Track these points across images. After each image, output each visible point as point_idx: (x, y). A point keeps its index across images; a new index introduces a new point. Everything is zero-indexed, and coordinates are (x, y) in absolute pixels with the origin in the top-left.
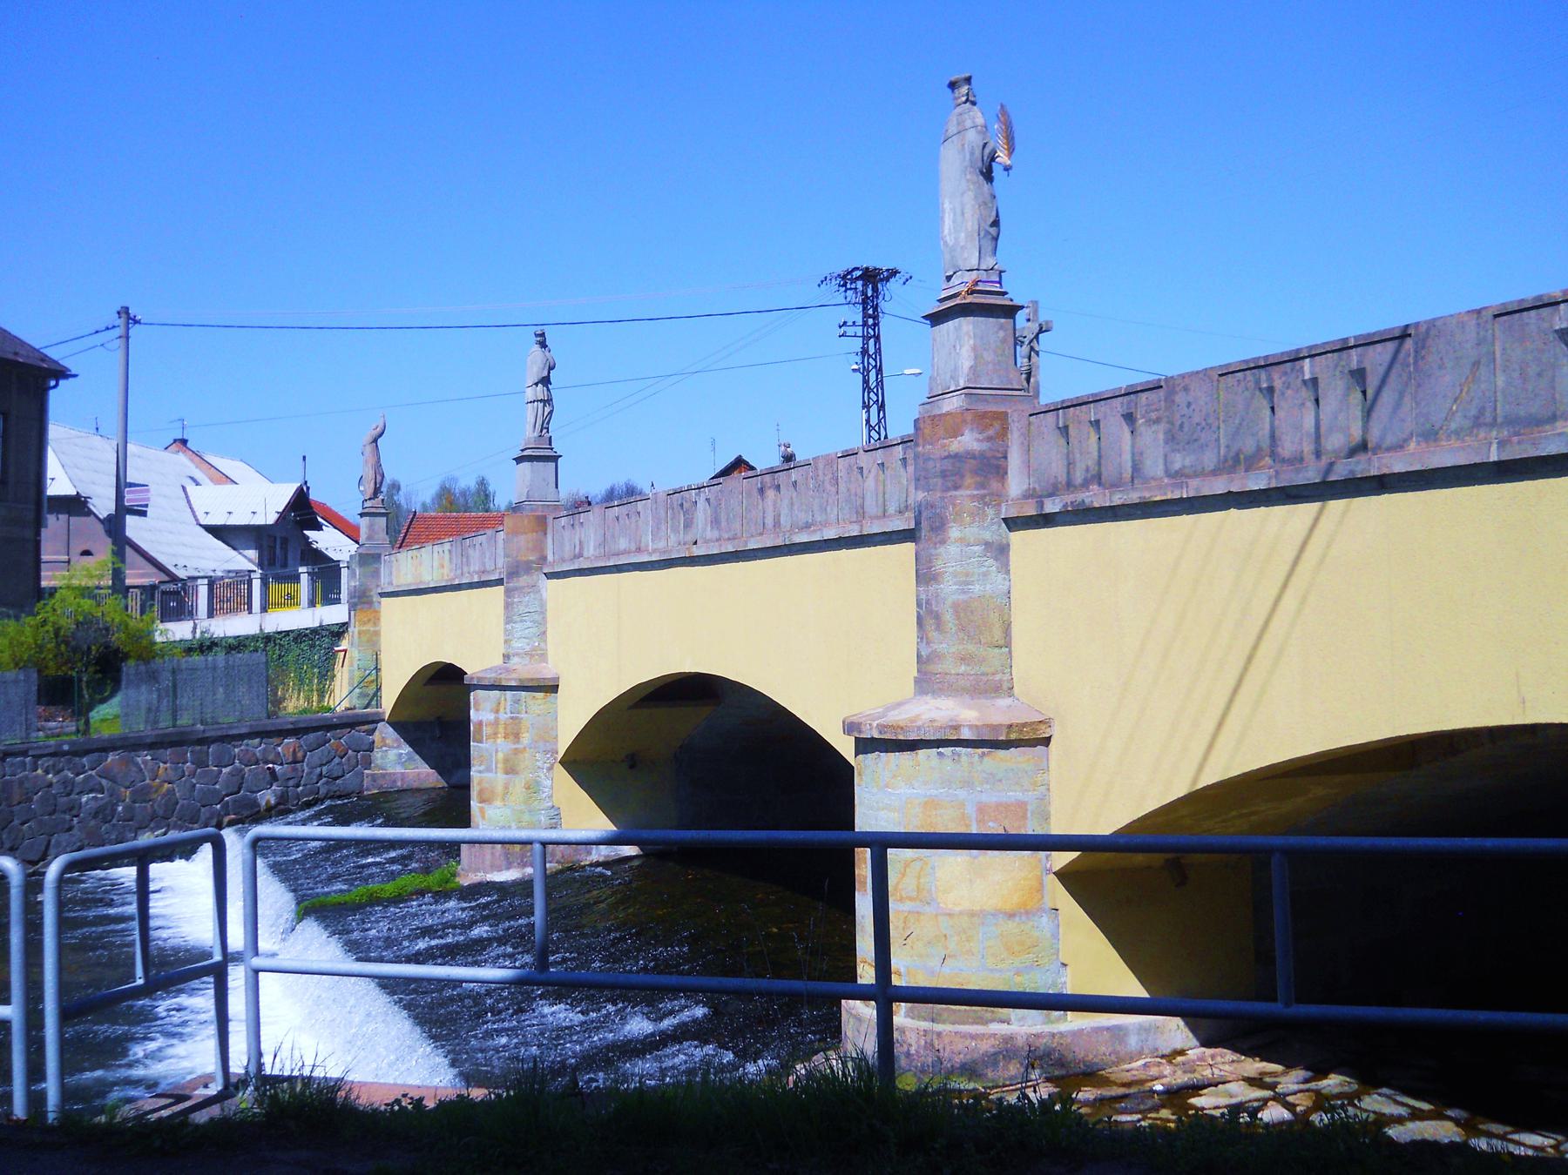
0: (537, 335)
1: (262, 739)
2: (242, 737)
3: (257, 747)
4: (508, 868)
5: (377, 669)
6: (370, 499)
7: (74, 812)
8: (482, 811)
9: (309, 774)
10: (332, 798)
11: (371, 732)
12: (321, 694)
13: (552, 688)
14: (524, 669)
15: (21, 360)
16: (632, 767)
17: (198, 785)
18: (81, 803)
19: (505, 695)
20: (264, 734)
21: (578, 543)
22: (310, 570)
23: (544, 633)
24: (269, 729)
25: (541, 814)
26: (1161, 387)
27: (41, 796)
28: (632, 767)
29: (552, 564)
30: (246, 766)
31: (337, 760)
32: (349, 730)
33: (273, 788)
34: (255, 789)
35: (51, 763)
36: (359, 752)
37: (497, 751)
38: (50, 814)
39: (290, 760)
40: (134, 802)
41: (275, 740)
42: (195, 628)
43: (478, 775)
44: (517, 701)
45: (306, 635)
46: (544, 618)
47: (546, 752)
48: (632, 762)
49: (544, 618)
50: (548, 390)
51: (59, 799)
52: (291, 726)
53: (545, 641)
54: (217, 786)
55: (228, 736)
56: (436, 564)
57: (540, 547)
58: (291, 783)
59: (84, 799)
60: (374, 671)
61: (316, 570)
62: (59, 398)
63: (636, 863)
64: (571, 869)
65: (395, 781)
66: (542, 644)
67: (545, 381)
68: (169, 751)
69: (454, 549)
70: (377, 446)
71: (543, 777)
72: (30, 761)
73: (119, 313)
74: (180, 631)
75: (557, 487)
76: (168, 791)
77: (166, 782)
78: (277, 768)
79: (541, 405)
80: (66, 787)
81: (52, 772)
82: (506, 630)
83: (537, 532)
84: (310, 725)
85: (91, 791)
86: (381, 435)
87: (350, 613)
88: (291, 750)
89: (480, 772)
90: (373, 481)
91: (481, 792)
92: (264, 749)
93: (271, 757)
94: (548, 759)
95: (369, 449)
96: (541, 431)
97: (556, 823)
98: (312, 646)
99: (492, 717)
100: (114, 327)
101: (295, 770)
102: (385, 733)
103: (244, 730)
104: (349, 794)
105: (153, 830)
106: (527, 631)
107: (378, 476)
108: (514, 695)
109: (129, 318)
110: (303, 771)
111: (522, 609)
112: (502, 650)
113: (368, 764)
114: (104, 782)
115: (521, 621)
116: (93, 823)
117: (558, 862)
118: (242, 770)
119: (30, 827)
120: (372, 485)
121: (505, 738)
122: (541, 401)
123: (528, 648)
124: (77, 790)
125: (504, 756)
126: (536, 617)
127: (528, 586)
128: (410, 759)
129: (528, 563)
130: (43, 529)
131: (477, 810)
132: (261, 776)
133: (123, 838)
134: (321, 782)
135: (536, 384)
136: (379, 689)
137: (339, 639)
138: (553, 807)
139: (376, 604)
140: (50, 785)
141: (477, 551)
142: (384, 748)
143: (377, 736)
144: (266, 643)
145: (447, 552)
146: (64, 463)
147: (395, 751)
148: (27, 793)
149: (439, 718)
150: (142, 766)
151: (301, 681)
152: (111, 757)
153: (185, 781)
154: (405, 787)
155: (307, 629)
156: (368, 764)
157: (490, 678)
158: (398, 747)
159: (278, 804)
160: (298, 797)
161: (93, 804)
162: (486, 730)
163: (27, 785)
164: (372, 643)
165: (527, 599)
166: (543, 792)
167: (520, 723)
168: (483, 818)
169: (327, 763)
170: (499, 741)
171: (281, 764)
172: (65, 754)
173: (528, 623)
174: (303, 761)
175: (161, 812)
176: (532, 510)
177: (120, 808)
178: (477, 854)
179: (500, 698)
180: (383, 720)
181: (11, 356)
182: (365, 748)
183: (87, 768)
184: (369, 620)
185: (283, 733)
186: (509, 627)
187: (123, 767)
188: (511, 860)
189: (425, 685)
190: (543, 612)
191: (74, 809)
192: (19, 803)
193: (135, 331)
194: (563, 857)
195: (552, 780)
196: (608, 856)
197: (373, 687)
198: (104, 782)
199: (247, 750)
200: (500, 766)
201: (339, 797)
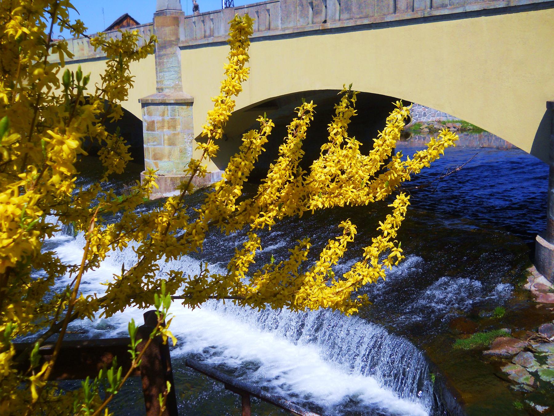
13: (190, 104)
23: (180, 77)
26: (395, 12)
29: (183, 42)
37: (164, 135)
44: (174, 110)
49: (180, 70)
53: (181, 81)
57: (176, 34)
66: (180, 83)
83: (174, 25)
94: (190, 137)
99: (160, 118)
106: (172, 76)
115: (169, 71)
121: (168, 128)
123: (173, 85)
126: (176, 69)
129: (170, 41)
157: (160, 99)
167: (176, 121)
170: (165, 130)
176: (171, 14)
179: (165, 109)
190: (179, 67)
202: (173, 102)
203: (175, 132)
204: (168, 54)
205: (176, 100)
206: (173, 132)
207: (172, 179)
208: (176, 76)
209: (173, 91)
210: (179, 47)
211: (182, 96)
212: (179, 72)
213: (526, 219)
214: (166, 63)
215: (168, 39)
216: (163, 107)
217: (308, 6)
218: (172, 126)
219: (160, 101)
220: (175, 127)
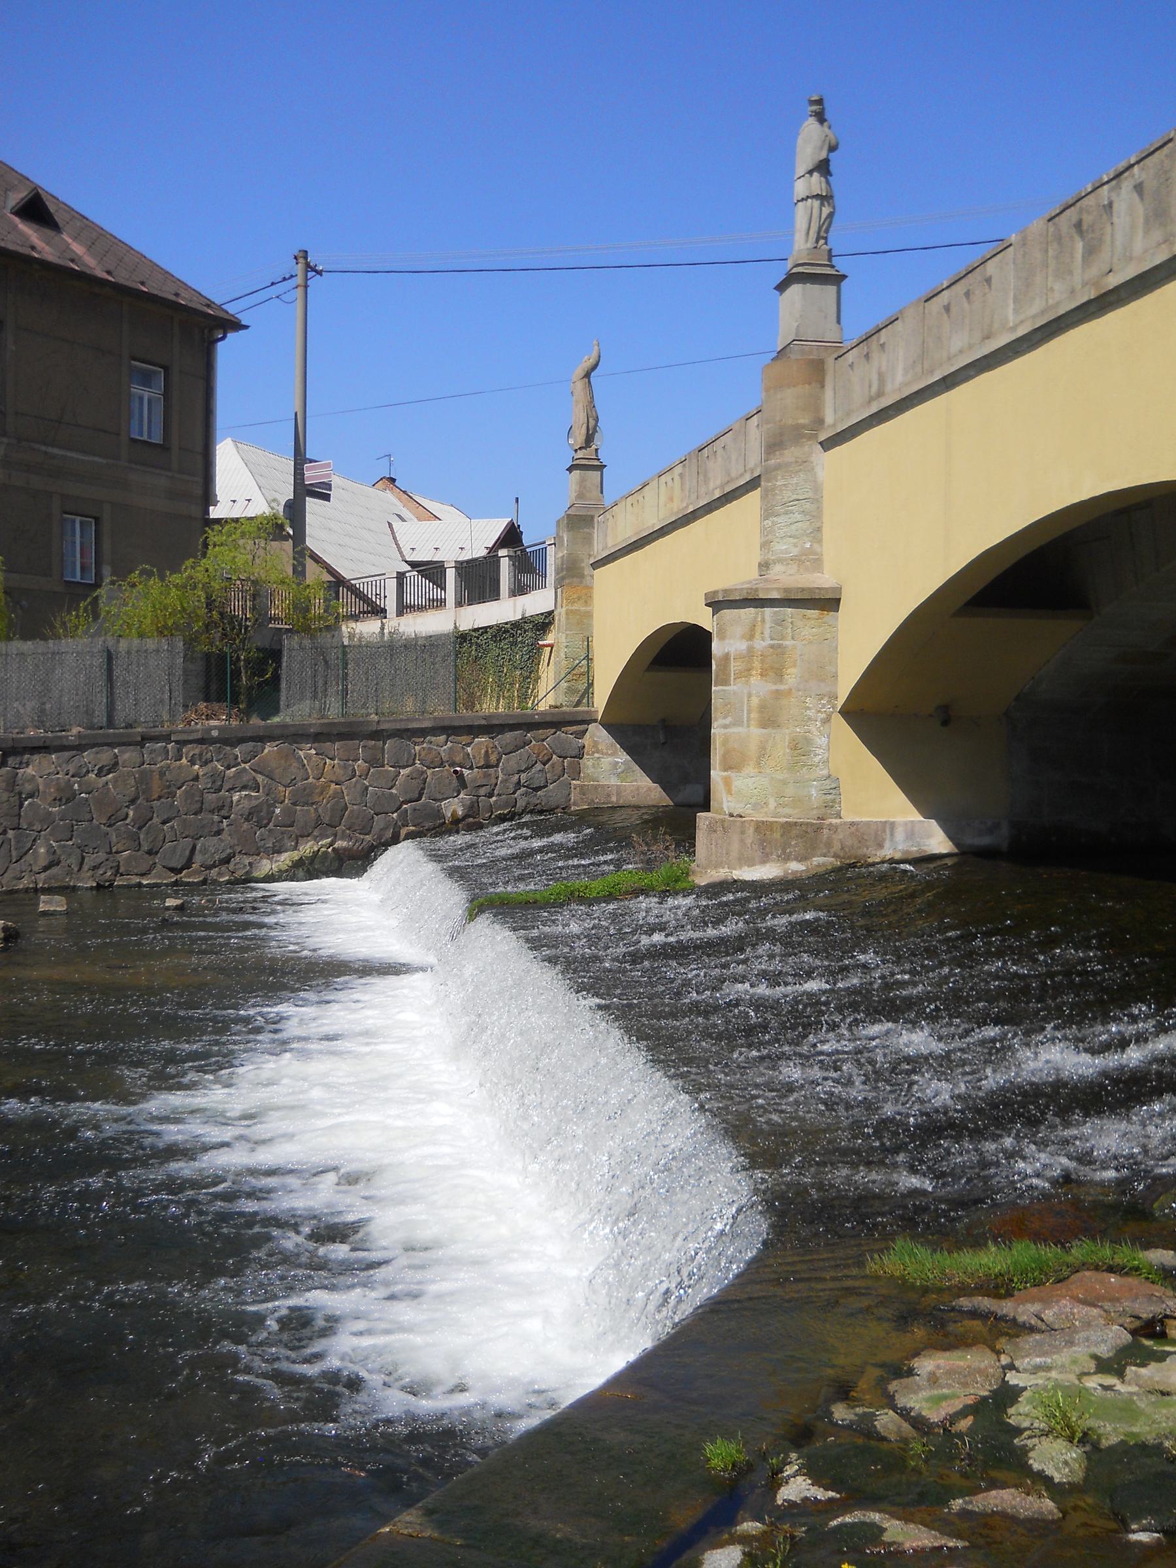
0: (812, 103)
1: (449, 736)
2: (423, 732)
3: (443, 746)
4: (764, 861)
5: (589, 659)
6: (580, 448)
7: (224, 812)
8: (727, 782)
9: (505, 781)
10: (531, 812)
11: (581, 734)
12: (524, 697)
14: (786, 578)
15: (183, 302)
16: (945, 723)
17: (370, 788)
18: (232, 801)
19: (763, 612)
20: (449, 730)
21: (875, 377)
22: (512, 554)
23: (819, 529)
24: (456, 724)
25: (812, 786)
27: (186, 792)
28: (945, 723)
30: (429, 768)
31: (539, 766)
32: (554, 730)
33: (461, 796)
34: (439, 797)
35: (197, 751)
36: (565, 758)
37: (750, 695)
38: (195, 814)
39: (482, 763)
40: (294, 804)
41: (465, 739)
42: (382, 628)
43: (723, 731)
44: (780, 622)
45: (506, 631)
46: (818, 508)
47: (821, 696)
48: (946, 716)
49: (819, 509)
50: (828, 182)
51: (205, 795)
52: (484, 722)
53: (820, 541)
54: (394, 791)
55: (408, 730)
56: (663, 499)
58: (482, 791)
59: (236, 797)
60: (584, 662)
61: (519, 553)
62: (228, 351)
63: (949, 862)
64: (853, 865)
65: (609, 795)
66: (816, 546)
67: (823, 167)
68: (337, 745)
69: (687, 470)
70: (589, 382)
71: (816, 733)
72: (172, 747)
73: (296, 258)
74: (369, 628)
75: (839, 322)
76: (335, 792)
77: (332, 782)
78: (466, 772)
79: (817, 203)
80: (214, 782)
81: (198, 762)
82: (763, 530)
83: (810, 384)
84: (506, 722)
85: (244, 788)
86: (595, 367)
87: (556, 593)
88: (483, 751)
89: (725, 727)
90: (585, 425)
91: (724, 758)
92: (451, 748)
93: (458, 759)
94: (824, 706)
95: (580, 385)
96: (817, 242)
97: (833, 801)
98: (514, 644)
99: (742, 646)
100: (292, 276)
101: (487, 776)
102: (597, 735)
103: (426, 724)
104: (553, 810)
105: (316, 839)
106: (794, 527)
107: (591, 420)
108: (775, 613)
109: (308, 265)
110: (497, 778)
111: (788, 495)
112: (757, 558)
113: (577, 773)
114: (260, 778)
115: (786, 513)
116: (246, 826)
117: (836, 856)
118: (423, 772)
119: (172, 827)
120: (584, 431)
121: (762, 675)
122: (817, 196)
123: (795, 551)
124: (226, 786)
125: (760, 700)
127: (796, 462)
128: (627, 770)
129: (798, 427)
130: (211, 508)
131: (719, 780)
132: (447, 781)
133: (281, 847)
134: (518, 792)
135: (810, 172)
136: (591, 685)
137: (544, 632)
138: (829, 776)
139: (588, 578)
140: (196, 778)
141: (719, 459)
142: (596, 755)
143: (586, 741)
144: (461, 643)
145: (677, 478)
146: (261, 485)
147: (610, 759)
148: (169, 786)
149: (663, 720)
150: (305, 762)
151: (501, 686)
152: (269, 748)
153: (357, 782)
154: (621, 802)
155: (506, 623)
156: (576, 774)
158: (614, 754)
159: (465, 817)
160: (491, 809)
161: (246, 804)
162: (734, 666)
163: (168, 776)
164: (583, 622)
165: (795, 480)
166: (816, 755)
168: (729, 792)
169: (527, 769)
170: (753, 680)
171: (471, 768)
172: (213, 741)
173: (796, 514)
174: (497, 766)
175: (326, 820)
177: (278, 811)
178: (720, 842)
180: (595, 721)
181: (173, 298)
182: (573, 754)
183: (239, 760)
184: (579, 598)
185: (473, 730)
186: (768, 523)
187: (283, 762)
188: (767, 850)
189: (646, 671)
190: (817, 500)
191: (223, 809)
192: (160, 798)
193: (315, 282)
194: (842, 848)
195: (828, 737)
196: (907, 852)
197: (582, 686)
198: (260, 778)
199: (430, 749)
200: (754, 715)
201: (541, 812)
202: (775, 595)
203: (781, 687)
204: (788, 465)
205: (786, 590)
206: (775, 687)
207: (760, 827)
208: (804, 525)
209: (792, 569)
210: (821, 443)
211: (814, 582)
212: (815, 515)
213: (823, 1290)
214: (781, 490)
215: (790, 422)
216: (749, 613)
217: (1071, 237)
218: (772, 668)
219: (744, 595)
220: (779, 675)
